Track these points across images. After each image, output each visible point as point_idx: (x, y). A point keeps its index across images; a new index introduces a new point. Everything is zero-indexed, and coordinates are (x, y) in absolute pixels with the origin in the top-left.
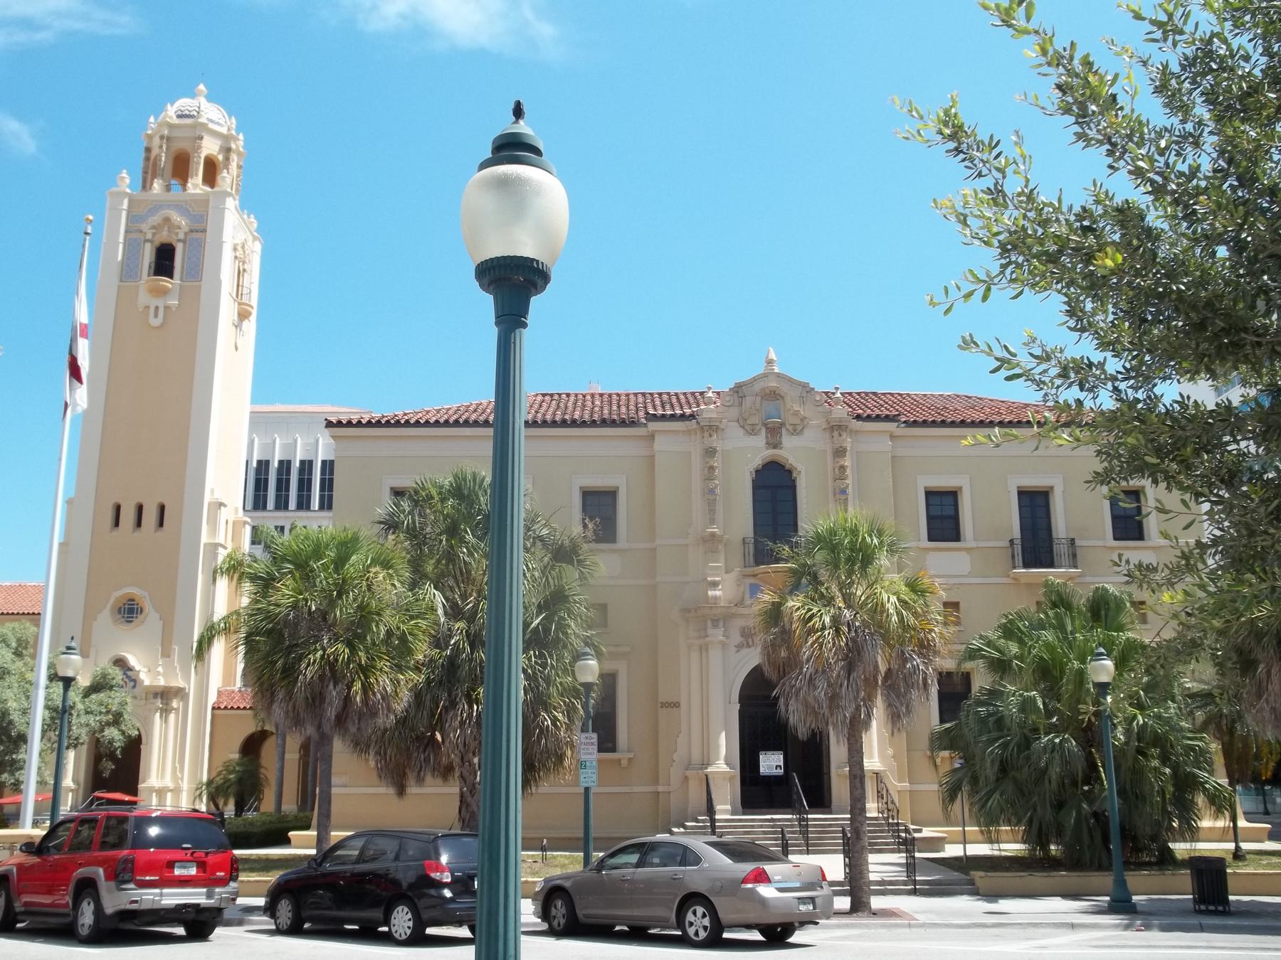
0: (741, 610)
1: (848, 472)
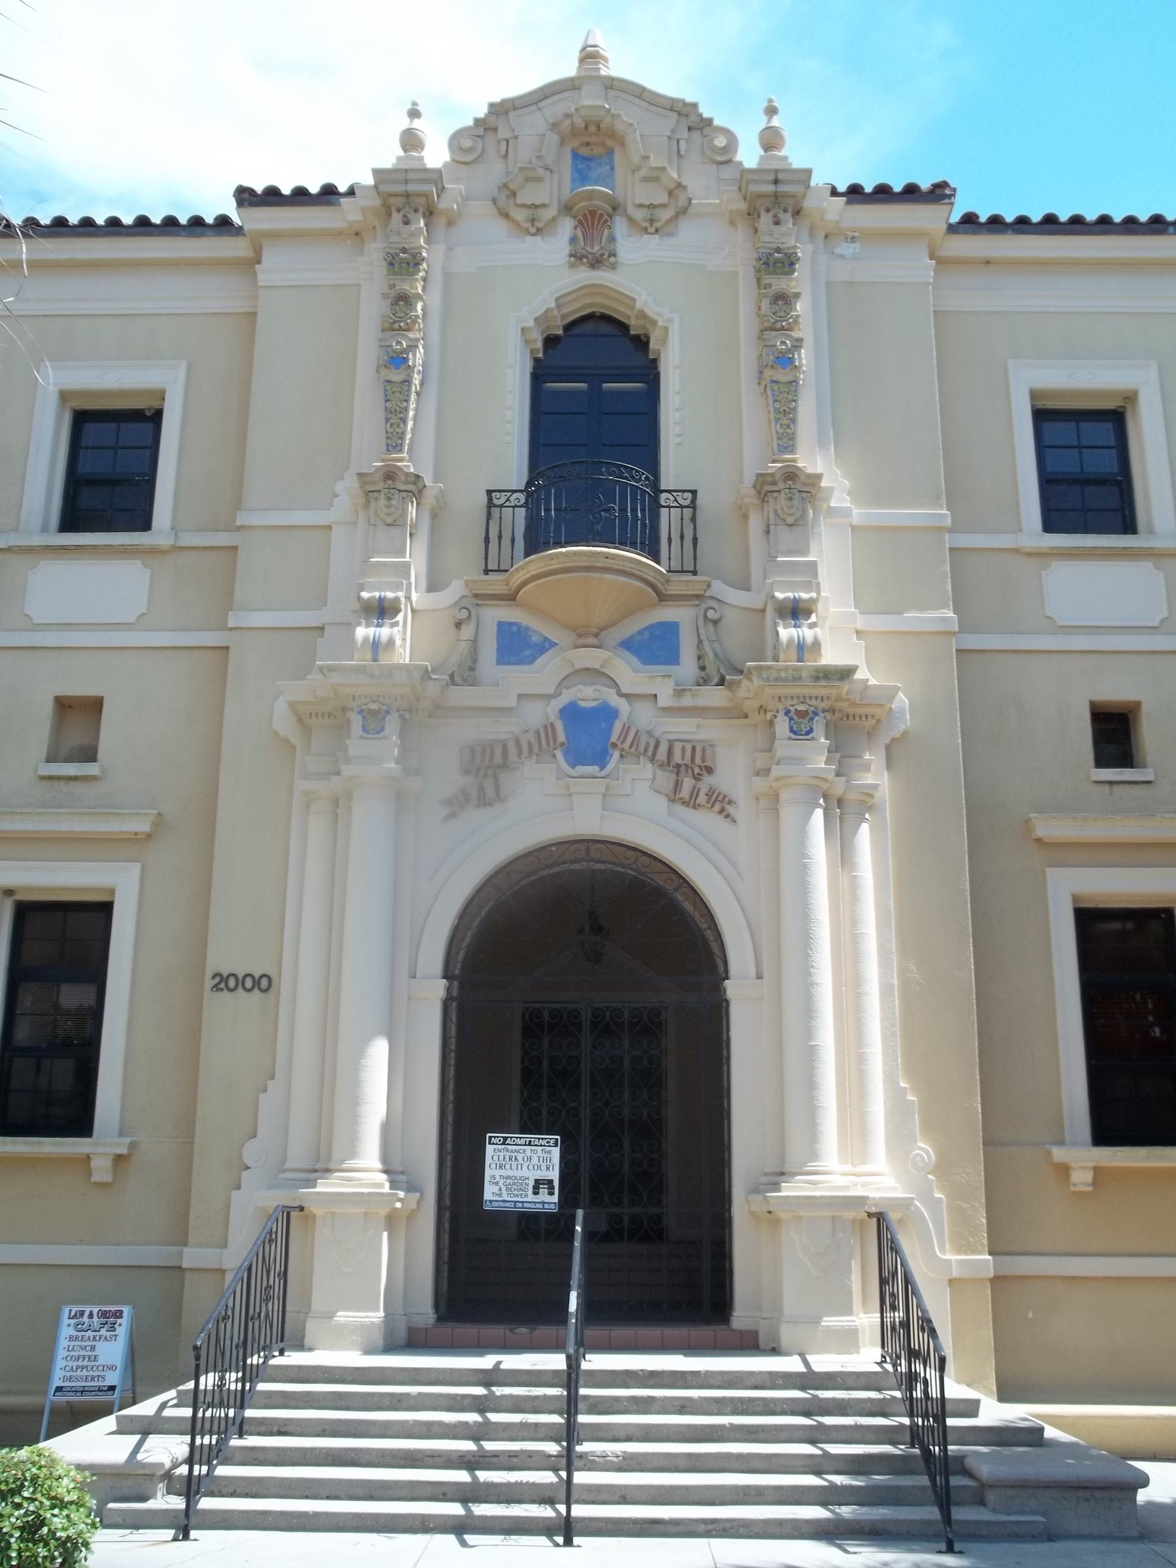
0: (462, 695)
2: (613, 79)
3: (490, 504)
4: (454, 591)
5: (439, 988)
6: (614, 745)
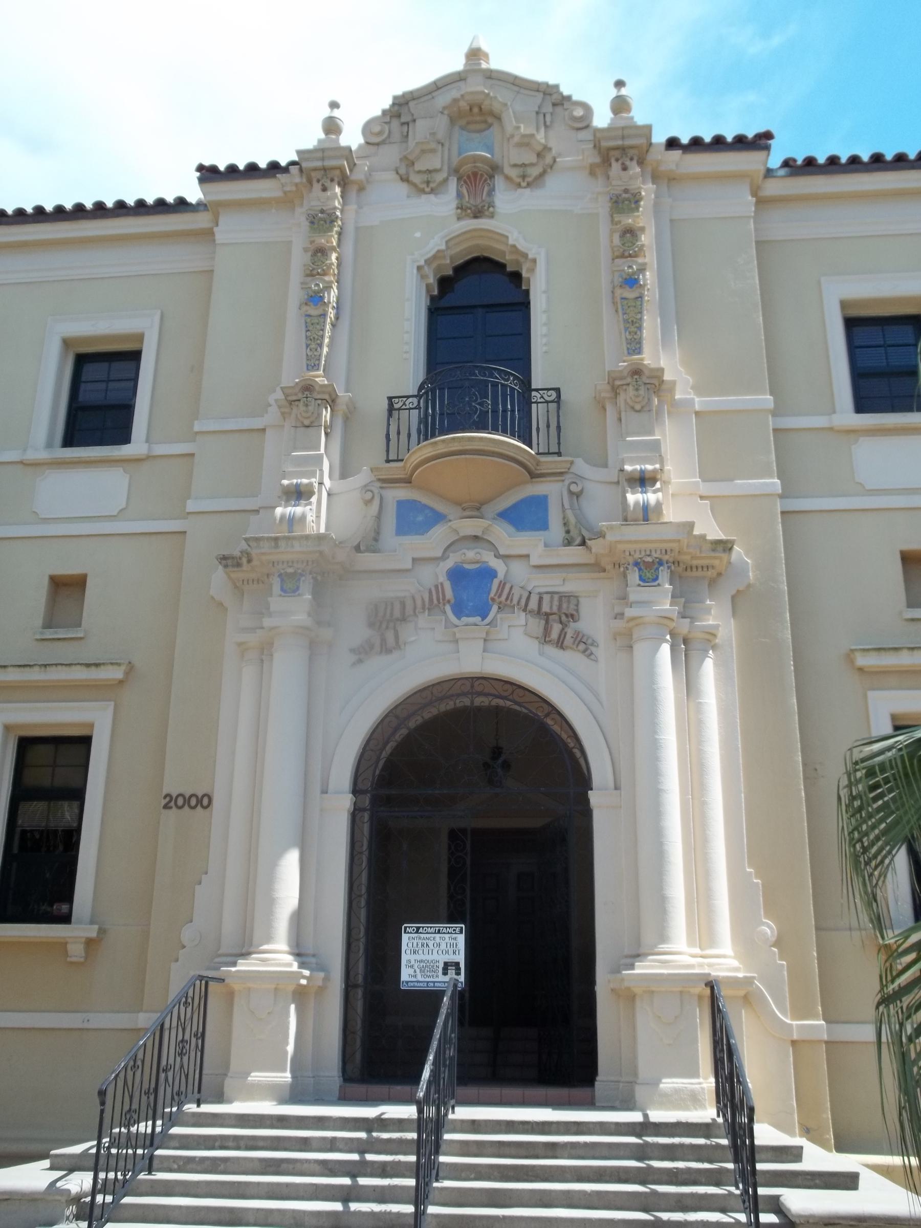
1: (645, 239)
2: (491, 71)
3: (391, 409)
4: (362, 477)
5: (346, 802)
6: (493, 599)
